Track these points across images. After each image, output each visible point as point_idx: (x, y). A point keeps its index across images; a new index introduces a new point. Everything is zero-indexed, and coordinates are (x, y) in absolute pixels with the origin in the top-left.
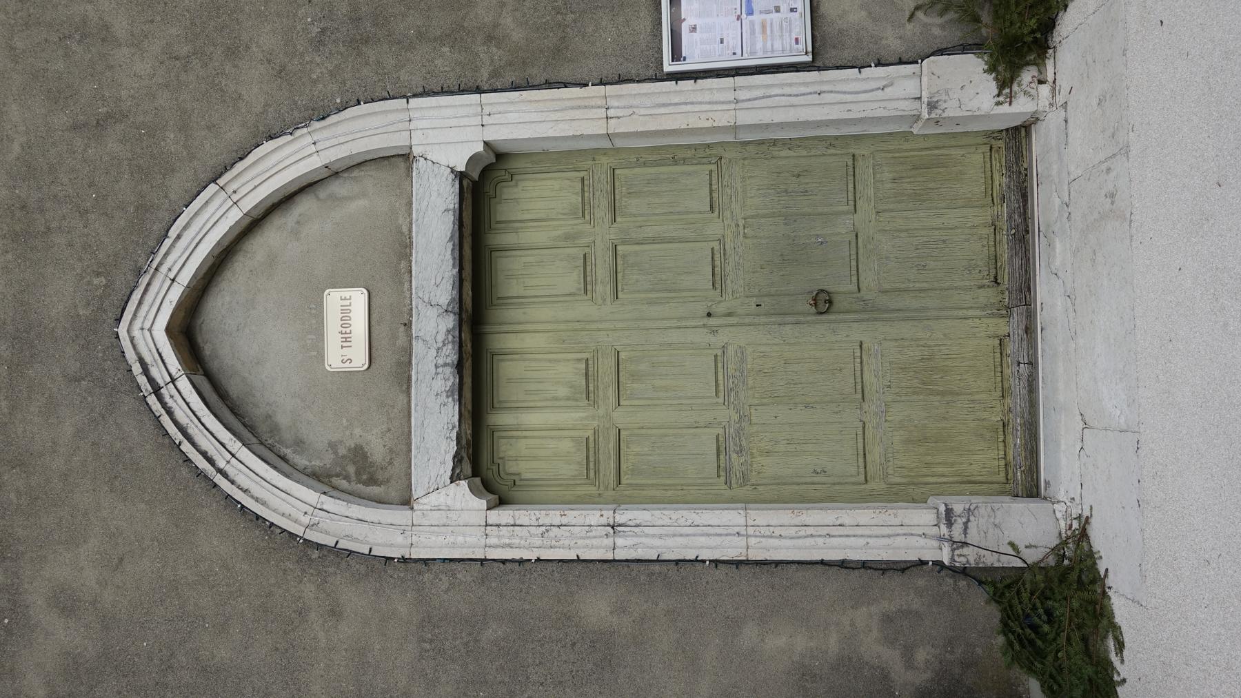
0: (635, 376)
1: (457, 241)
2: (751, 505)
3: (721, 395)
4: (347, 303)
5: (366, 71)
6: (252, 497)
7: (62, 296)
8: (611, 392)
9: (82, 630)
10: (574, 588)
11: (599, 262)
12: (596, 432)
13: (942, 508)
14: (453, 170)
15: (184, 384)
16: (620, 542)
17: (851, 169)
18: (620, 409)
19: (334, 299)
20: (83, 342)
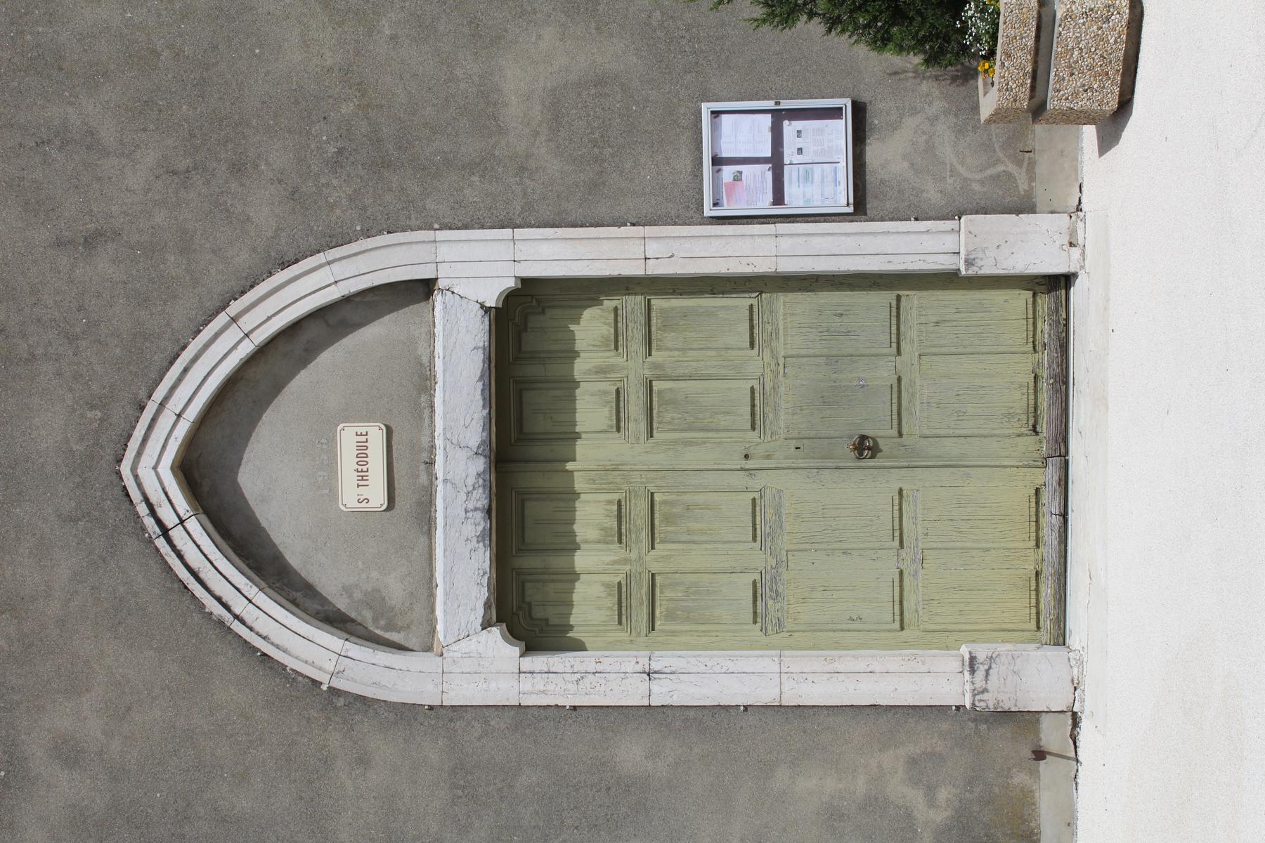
0: (668, 519)
1: (487, 380)
2: (787, 653)
3: (759, 539)
4: (363, 439)
5: (388, 198)
6: (272, 644)
7: (50, 427)
8: (644, 535)
9: (88, 781)
10: (610, 734)
11: (633, 398)
12: (629, 576)
13: (967, 657)
14: (482, 306)
15: (193, 525)
16: (656, 688)
17: (894, 310)
18: (653, 552)
19: (347, 437)
20: (78, 479)
